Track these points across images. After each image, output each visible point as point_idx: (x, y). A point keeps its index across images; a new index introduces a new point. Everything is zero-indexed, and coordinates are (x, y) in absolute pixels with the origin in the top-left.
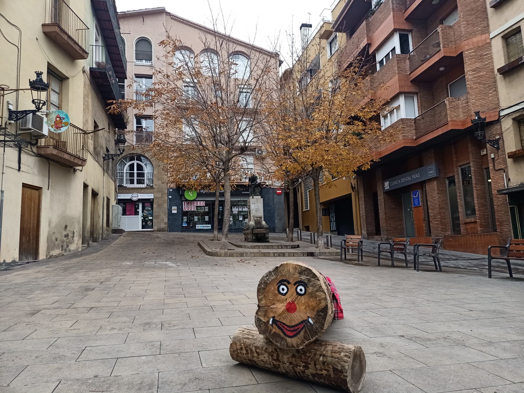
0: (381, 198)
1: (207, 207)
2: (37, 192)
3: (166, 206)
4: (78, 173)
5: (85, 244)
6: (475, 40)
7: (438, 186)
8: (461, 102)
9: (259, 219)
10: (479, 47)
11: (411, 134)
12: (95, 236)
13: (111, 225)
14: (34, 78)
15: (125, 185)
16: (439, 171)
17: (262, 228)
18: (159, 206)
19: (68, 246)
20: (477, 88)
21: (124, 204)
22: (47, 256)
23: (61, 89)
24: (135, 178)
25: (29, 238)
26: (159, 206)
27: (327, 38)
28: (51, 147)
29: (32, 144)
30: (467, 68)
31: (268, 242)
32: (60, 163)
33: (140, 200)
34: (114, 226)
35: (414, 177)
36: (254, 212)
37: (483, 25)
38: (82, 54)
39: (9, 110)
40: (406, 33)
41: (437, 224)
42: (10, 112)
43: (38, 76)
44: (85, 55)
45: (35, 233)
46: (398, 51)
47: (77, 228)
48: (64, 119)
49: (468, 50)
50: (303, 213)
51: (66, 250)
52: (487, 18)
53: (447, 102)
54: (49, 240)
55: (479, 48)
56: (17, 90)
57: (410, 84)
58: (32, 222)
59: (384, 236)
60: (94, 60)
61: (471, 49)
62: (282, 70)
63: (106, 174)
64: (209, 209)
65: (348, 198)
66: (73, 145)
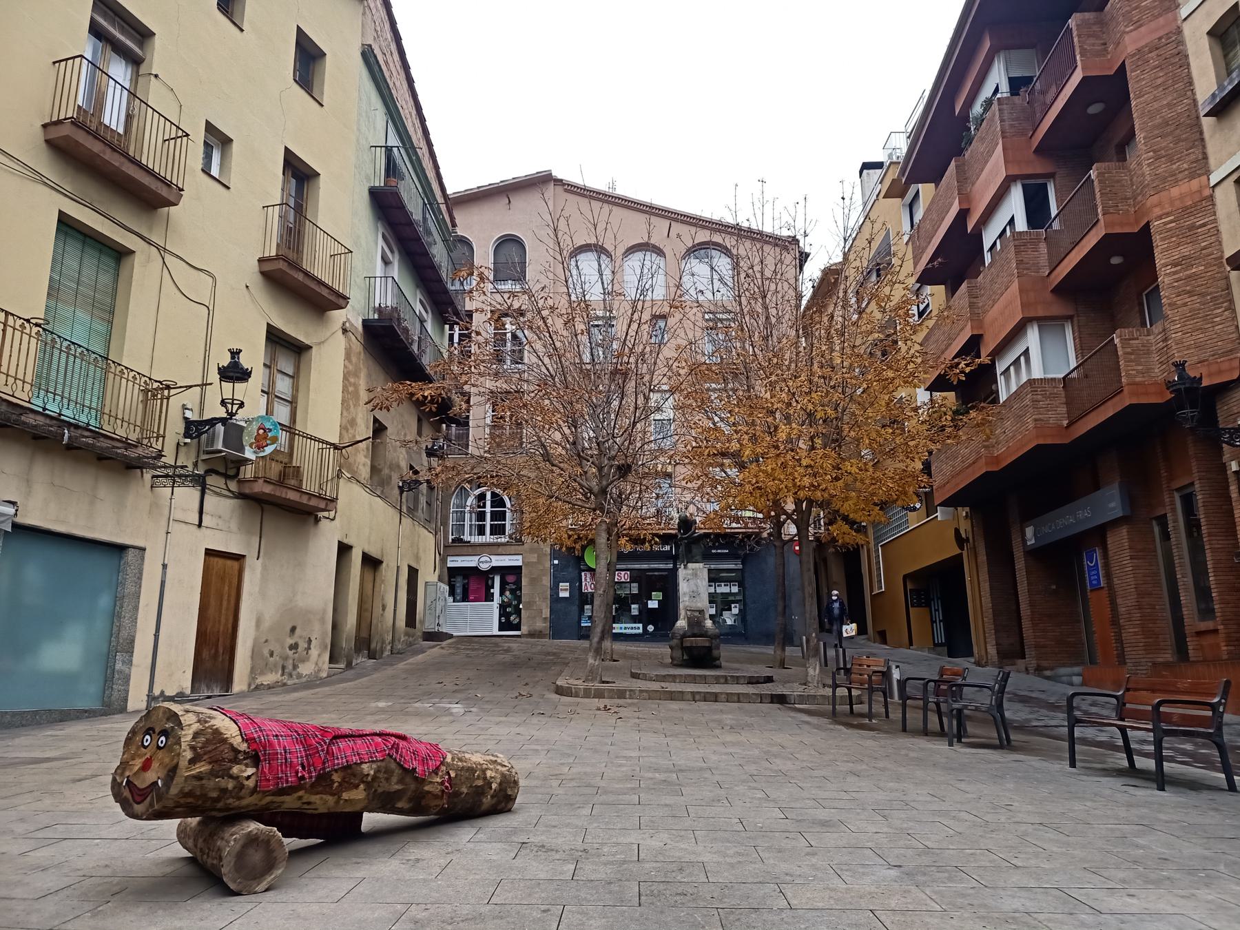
0: (1020, 564)
1: (635, 585)
2: (236, 564)
3: (547, 581)
4: (324, 524)
5: (337, 662)
6: (1175, 192)
7: (1131, 540)
8: (1154, 339)
9: (697, 614)
10: (1185, 208)
11: (1058, 415)
12: (373, 646)
13: (422, 622)
14: (226, 360)
15: (466, 537)
16: (1130, 499)
17: (704, 634)
18: (534, 581)
19: (295, 667)
20: (1185, 305)
21: (465, 577)
22: (249, 685)
23: (297, 368)
24: (488, 522)
25: (217, 651)
26: (534, 581)
27: (902, 196)
28: (261, 481)
29: (227, 477)
30: (1159, 260)
31: (719, 667)
32: (284, 507)
33: (495, 570)
34: (430, 626)
35: (1081, 515)
36: (687, 598)
37: (1193, 157)
38: (340, 301)
39: (186, 419)
40: (1040, 181)
41: (1136, 634)
42: (188, 422)
43: (233, 358)
44: (341, 302)
45: (228, 642)
46: (1021, 225)
47: (320, 632)
48: (270, 430)
49: (1160, 218)
50: (873, 597)
51: (291, 675)
52: (1203, 140)
53: (1117, 341)
54: (255, 654)
55: (1186, 211)
56: (203, 385)
57: (1048, 296)
58: (223, 620)
59: (1031, 660)
60: (372, 305)
61: (1168, 214)
62: (813, 270)
63: (407, 521)
64: (640, 589)
65: (956, 562)
66: (313, 467)
